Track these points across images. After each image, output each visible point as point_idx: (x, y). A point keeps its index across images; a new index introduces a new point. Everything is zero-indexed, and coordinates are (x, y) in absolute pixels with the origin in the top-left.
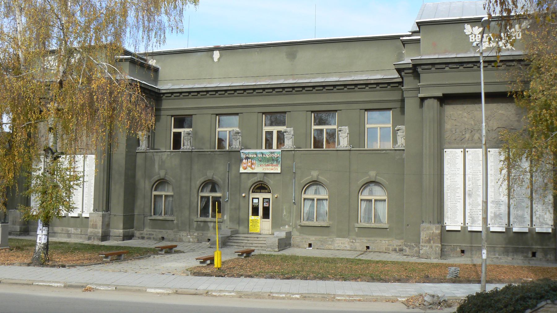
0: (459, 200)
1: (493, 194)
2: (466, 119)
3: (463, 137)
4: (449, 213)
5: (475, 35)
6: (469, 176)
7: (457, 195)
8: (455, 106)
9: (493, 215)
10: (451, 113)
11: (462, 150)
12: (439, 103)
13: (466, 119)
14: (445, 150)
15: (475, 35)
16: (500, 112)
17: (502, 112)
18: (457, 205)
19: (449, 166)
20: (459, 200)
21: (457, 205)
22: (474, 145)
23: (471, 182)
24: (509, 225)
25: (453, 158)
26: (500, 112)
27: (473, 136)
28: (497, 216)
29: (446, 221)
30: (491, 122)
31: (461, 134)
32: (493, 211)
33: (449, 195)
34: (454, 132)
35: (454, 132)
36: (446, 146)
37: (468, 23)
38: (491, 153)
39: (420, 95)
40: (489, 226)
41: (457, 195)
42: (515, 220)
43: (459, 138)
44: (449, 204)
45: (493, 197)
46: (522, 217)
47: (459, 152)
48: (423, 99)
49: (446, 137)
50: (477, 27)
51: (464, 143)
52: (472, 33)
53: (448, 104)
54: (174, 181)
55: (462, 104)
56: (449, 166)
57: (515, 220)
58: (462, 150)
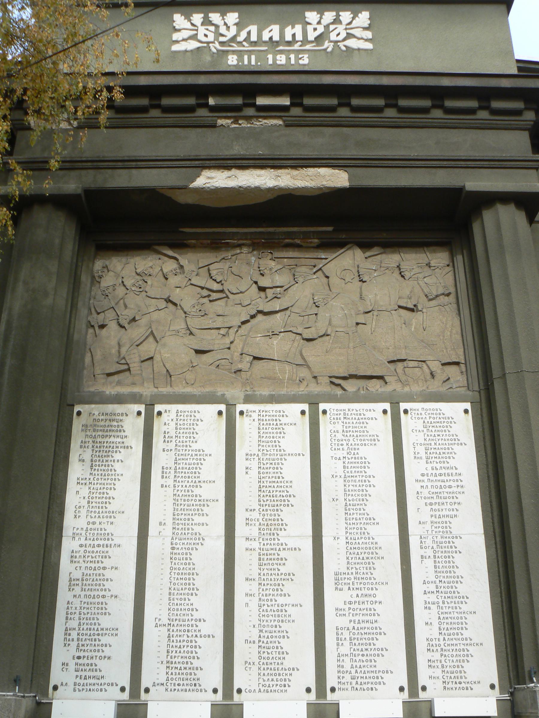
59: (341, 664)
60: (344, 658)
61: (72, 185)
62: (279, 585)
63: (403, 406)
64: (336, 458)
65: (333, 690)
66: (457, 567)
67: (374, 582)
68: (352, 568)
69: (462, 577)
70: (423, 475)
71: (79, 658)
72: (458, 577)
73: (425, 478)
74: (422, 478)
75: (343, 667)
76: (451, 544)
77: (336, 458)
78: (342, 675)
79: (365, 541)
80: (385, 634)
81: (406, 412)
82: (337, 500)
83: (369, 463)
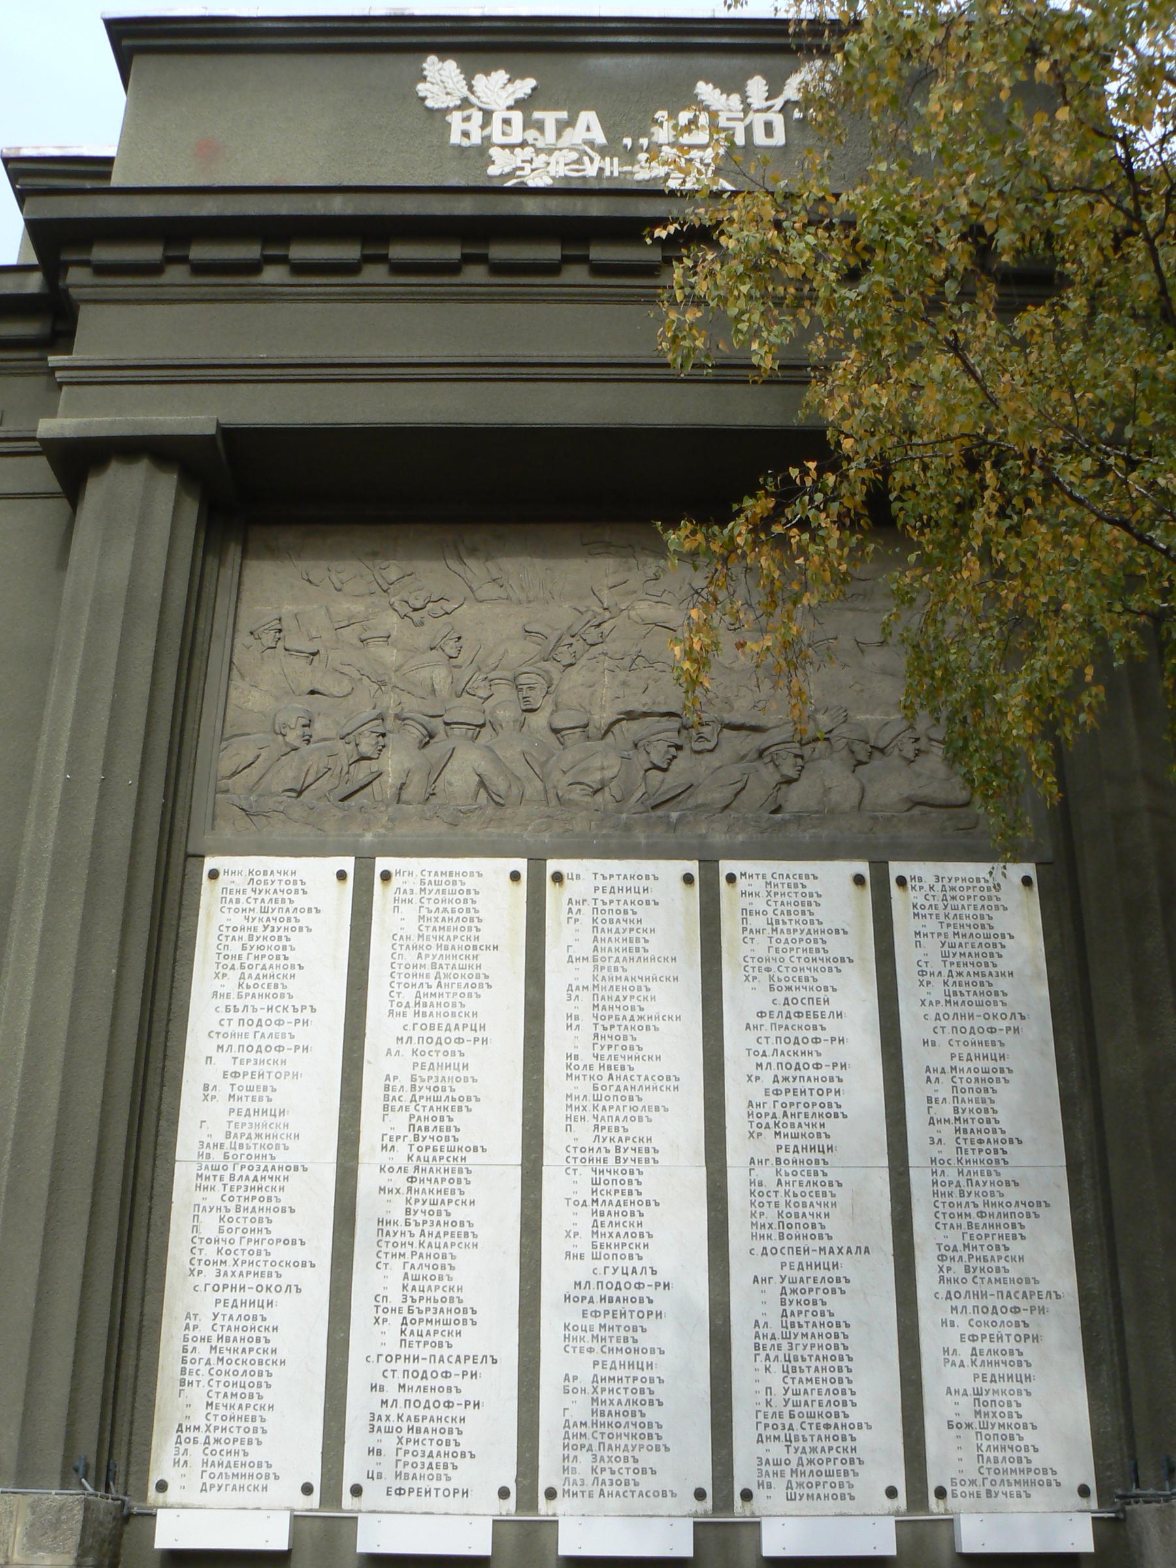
0: (290, 1276)
1: (585, 1219)
2: (391, 656)
3: (362, 772)
4: (197, 1395)
5: (487, 114)
6: (390, 1066)
7: (281, 1226)
8: (318, 569)
9: (580, 1409)
10: (288, 609)
11: (348, 863)
12: (191, 510)
13: (391, 656)
14: (210, 863)
15: (487, 114)
16: (644, 609)
17: (660, 612)
18: (273, 1316)
19: (230, 984)
20: (290, 1276)
21: (273, 1316)
22: (437, 827)
23: (399, 1123)
24: (723, 1501)
25: (265, 926)
26: (644, 609)
27: (436, 771)
28: (623, 1422)
29: (164, 1462)
30: (576, 676)
31: (345, 751)
32: (584, 1368)
33: (209, 1225)
34: (293, 737)
35: (293, 737)
36: (226, 832)
37: (444, 51)
38: (571, 888)
39: (57, 425)
40: (545, 1507)
41: (281, 1226)
42: (777, 1450)
43: (325, 783)
44: (206, 1305)
45: (583, 1244)
46: (833, 1422)
47: (320, 881)
48: (76, 463)
49: (226, 765)
50: (500, 76)
51: (356, 812)
52: (465, 104)
53: (273, 552)
54: (1104, 1368)
55: (374, 555)
56: (230, 984)
57: (777, 1450)
58: (348, 863)
59: (571, 1465)
60: (580, 993)
61: (191, 415)
62: (451, 1432)
63: (726, 866)
64: (576, 1203)
65: (551, 1494)
66: (861, 1462)
67: (640, 1105)
68: (603, 1470)
69: (847, 1326)
70: (761, 1014)
71: (236, 1074)
72: (838, 1325)
73: (767, 1021)
74: (759, 1021)
75: (574, 1470)
76: (841, 1351)
77: (576, 1203)
78: (572, 1453)
79: (635, 1397)
80: (660, 1404)
81: (731, 878)
82: (576, 1234)
83: (656, 1151)
